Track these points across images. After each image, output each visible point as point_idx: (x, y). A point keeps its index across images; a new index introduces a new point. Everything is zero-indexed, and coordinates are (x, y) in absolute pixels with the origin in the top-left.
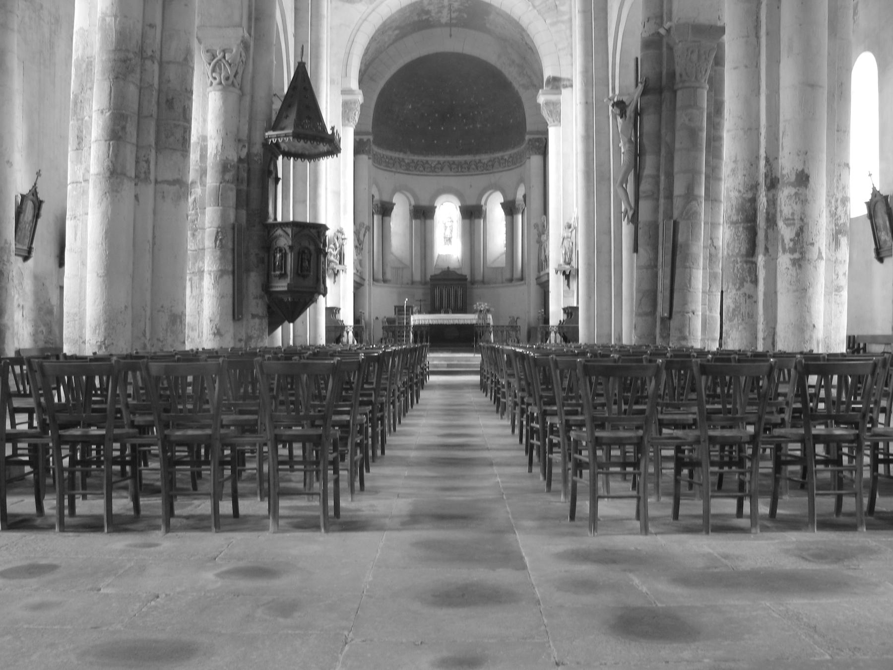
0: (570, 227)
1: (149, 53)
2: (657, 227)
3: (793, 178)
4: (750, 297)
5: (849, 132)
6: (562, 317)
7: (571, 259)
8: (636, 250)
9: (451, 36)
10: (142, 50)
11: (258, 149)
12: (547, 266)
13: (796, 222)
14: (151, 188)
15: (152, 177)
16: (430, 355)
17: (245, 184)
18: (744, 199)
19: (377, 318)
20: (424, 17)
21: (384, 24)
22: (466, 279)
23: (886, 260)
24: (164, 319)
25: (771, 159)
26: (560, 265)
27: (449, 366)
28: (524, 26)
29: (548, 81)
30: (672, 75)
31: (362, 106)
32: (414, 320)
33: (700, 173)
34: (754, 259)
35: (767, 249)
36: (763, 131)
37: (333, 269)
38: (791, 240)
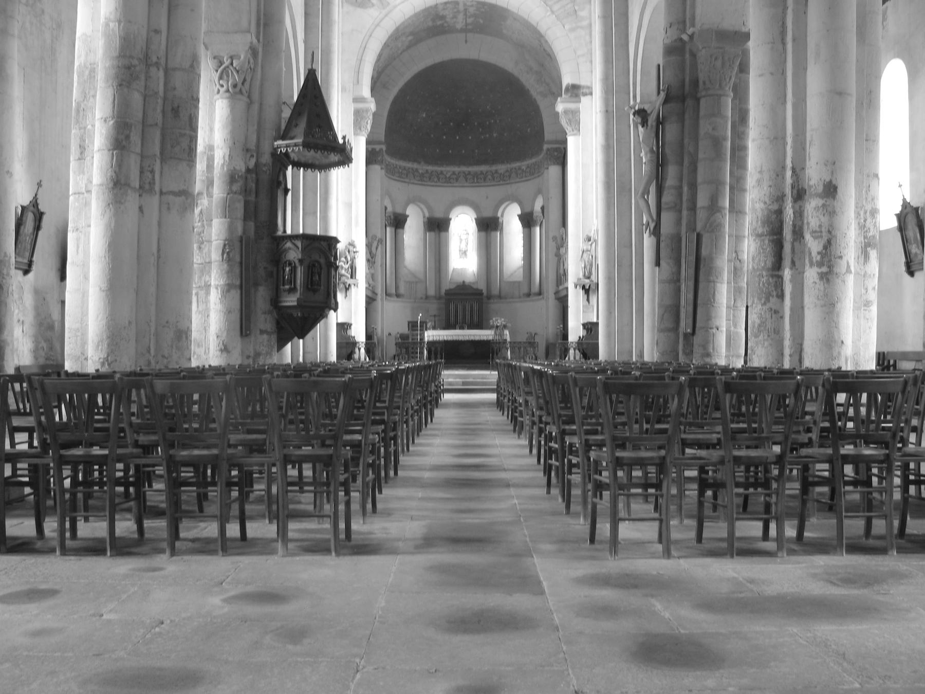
0: (589, 240)
1: (154, 59)
3: (820, 189)
4: (776, 312)
5: (878, 141)
6: (581, 332)
7: (590, 273)
8: (658, 263)
9: (466, 41)
10: (147, 56)
11: (266, 158)
12: (566, 280)
13: (824, 234)
15: (157, 188)
16: (445, 373)
17: (254, 195)
18: (770, 210)
19: (390, 334)
20: (439, 23)
23: (917, 274)
26: (579, 279)
27: (464, 383)
28: (542, 32)
29: (567, 89)
30: (695, 83)
31: (374, 114)
32: (428, 336)
33: (724, 183)
34: (780, 273)
35: (793, 263)
36: (789, 140)
37: (344, 283)
38: (819, 253)
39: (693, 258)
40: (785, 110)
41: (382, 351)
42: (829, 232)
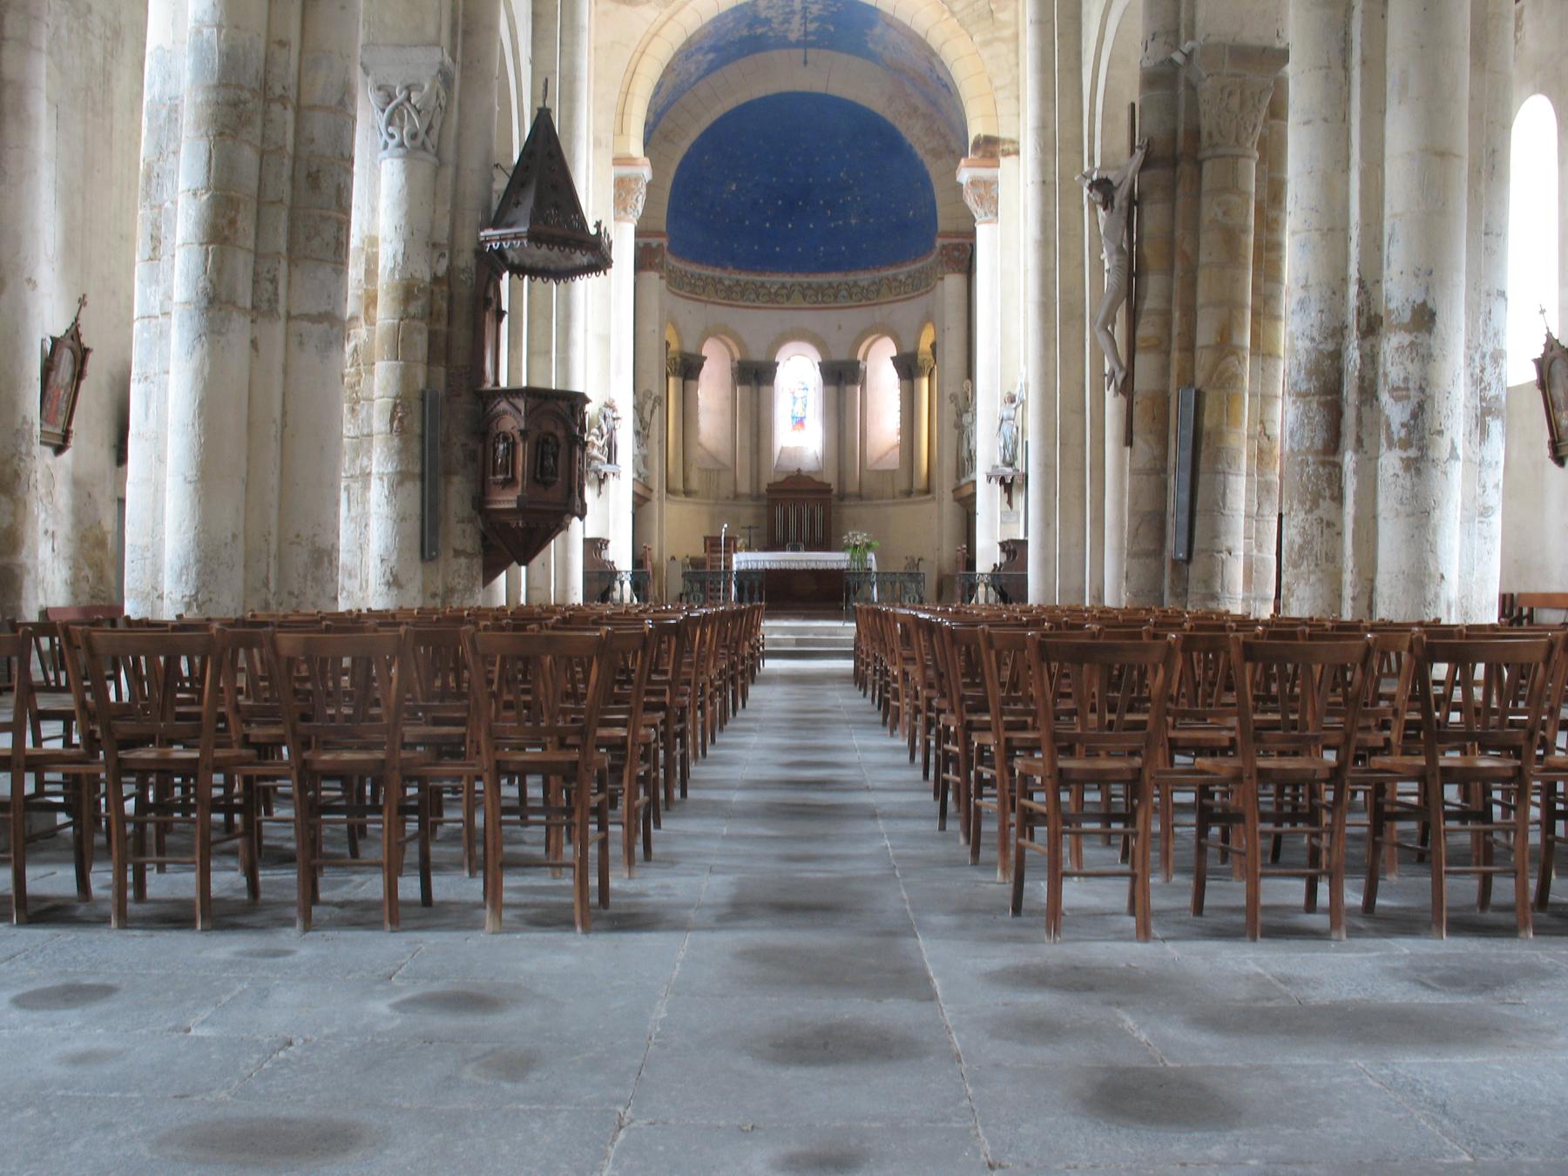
1: (278, 91)
2: (1167, 401)
3: (1407, 316)
4: (1329, 524)
6: (998, 557)
7: (1014, 456)
8: (1129, 441)
9: (805, 63)
10: (265, 86)
11: (466, 259)
12: (973, 468)
13: (1412, 393)
14: (279, 328)
15: (282, 309)
16: (766, 624)
17: (444, 321)
18: (1321, 352)
19: (673, 558)
20: (759, 31)
21: (689, 42)
22: (830, 491)
24: (301, 557)
25: (1368, 284)
26: (995, 467)
27: (799, 642)
29: (977, 144)
30: (1195, 135)
31: (649, 185)
32: (739, 562)
33: (1242, 306)
34: (1337, 459)
35: (1359, 441)
36: (1355, 233)
37: (597, 472)
38: (1403, 425)
39: (1188, 433)
40: (1347, 183)
41: (660, 588)
42: (1422, 390)
